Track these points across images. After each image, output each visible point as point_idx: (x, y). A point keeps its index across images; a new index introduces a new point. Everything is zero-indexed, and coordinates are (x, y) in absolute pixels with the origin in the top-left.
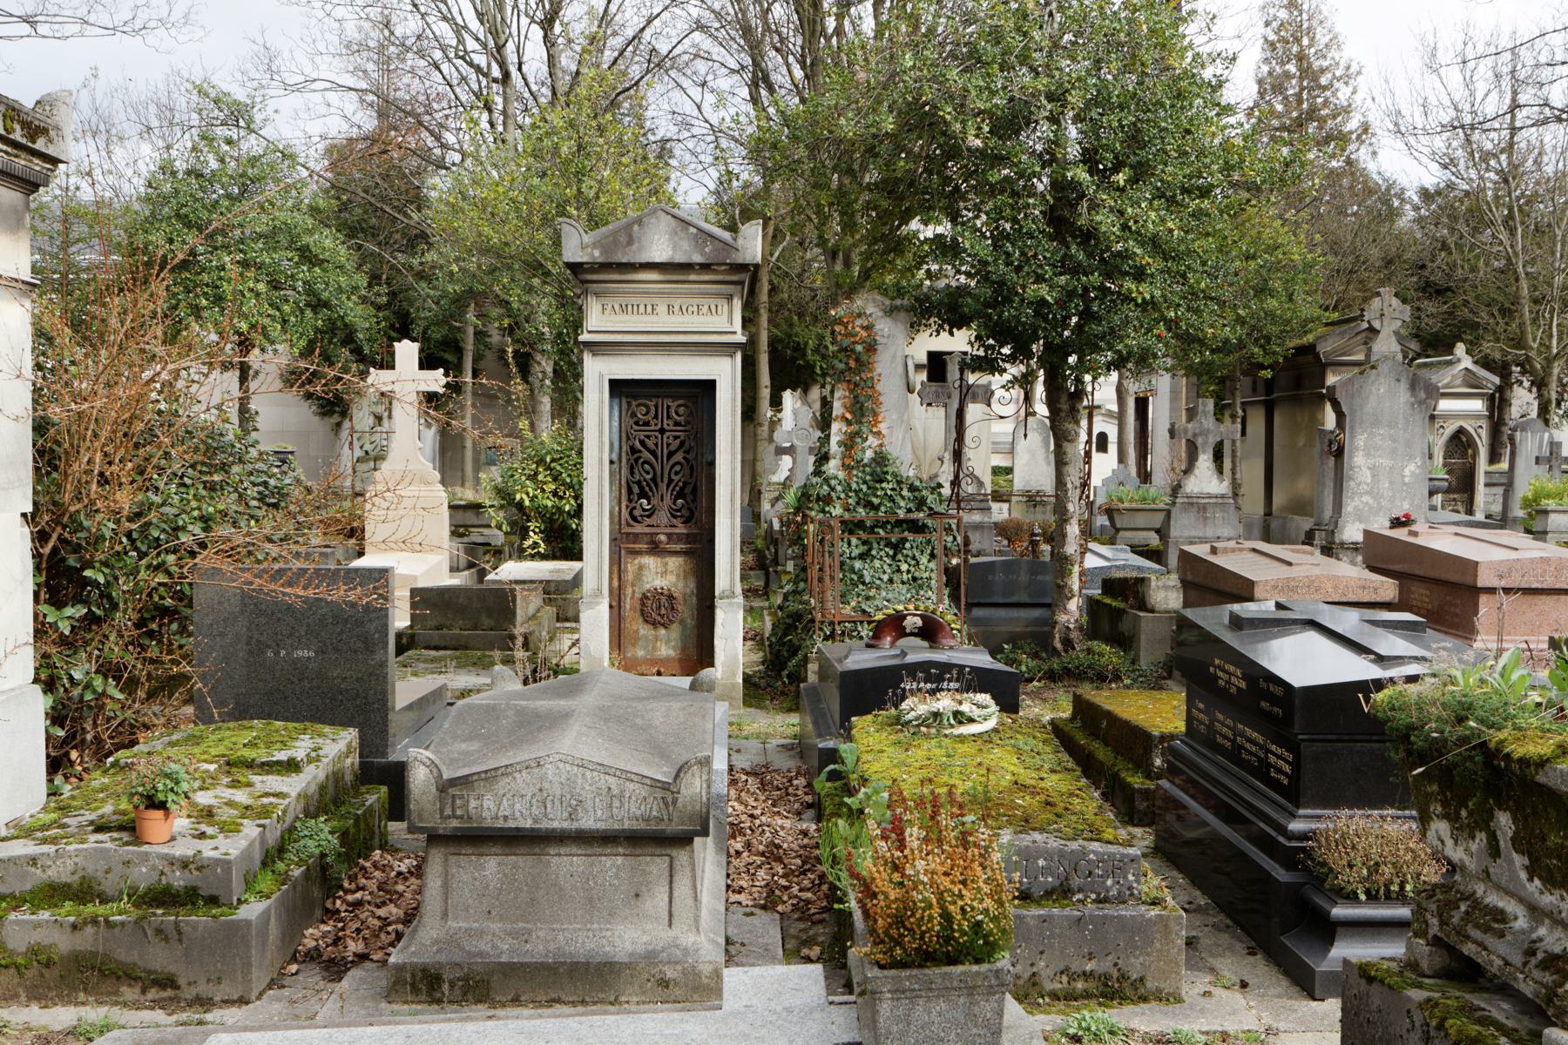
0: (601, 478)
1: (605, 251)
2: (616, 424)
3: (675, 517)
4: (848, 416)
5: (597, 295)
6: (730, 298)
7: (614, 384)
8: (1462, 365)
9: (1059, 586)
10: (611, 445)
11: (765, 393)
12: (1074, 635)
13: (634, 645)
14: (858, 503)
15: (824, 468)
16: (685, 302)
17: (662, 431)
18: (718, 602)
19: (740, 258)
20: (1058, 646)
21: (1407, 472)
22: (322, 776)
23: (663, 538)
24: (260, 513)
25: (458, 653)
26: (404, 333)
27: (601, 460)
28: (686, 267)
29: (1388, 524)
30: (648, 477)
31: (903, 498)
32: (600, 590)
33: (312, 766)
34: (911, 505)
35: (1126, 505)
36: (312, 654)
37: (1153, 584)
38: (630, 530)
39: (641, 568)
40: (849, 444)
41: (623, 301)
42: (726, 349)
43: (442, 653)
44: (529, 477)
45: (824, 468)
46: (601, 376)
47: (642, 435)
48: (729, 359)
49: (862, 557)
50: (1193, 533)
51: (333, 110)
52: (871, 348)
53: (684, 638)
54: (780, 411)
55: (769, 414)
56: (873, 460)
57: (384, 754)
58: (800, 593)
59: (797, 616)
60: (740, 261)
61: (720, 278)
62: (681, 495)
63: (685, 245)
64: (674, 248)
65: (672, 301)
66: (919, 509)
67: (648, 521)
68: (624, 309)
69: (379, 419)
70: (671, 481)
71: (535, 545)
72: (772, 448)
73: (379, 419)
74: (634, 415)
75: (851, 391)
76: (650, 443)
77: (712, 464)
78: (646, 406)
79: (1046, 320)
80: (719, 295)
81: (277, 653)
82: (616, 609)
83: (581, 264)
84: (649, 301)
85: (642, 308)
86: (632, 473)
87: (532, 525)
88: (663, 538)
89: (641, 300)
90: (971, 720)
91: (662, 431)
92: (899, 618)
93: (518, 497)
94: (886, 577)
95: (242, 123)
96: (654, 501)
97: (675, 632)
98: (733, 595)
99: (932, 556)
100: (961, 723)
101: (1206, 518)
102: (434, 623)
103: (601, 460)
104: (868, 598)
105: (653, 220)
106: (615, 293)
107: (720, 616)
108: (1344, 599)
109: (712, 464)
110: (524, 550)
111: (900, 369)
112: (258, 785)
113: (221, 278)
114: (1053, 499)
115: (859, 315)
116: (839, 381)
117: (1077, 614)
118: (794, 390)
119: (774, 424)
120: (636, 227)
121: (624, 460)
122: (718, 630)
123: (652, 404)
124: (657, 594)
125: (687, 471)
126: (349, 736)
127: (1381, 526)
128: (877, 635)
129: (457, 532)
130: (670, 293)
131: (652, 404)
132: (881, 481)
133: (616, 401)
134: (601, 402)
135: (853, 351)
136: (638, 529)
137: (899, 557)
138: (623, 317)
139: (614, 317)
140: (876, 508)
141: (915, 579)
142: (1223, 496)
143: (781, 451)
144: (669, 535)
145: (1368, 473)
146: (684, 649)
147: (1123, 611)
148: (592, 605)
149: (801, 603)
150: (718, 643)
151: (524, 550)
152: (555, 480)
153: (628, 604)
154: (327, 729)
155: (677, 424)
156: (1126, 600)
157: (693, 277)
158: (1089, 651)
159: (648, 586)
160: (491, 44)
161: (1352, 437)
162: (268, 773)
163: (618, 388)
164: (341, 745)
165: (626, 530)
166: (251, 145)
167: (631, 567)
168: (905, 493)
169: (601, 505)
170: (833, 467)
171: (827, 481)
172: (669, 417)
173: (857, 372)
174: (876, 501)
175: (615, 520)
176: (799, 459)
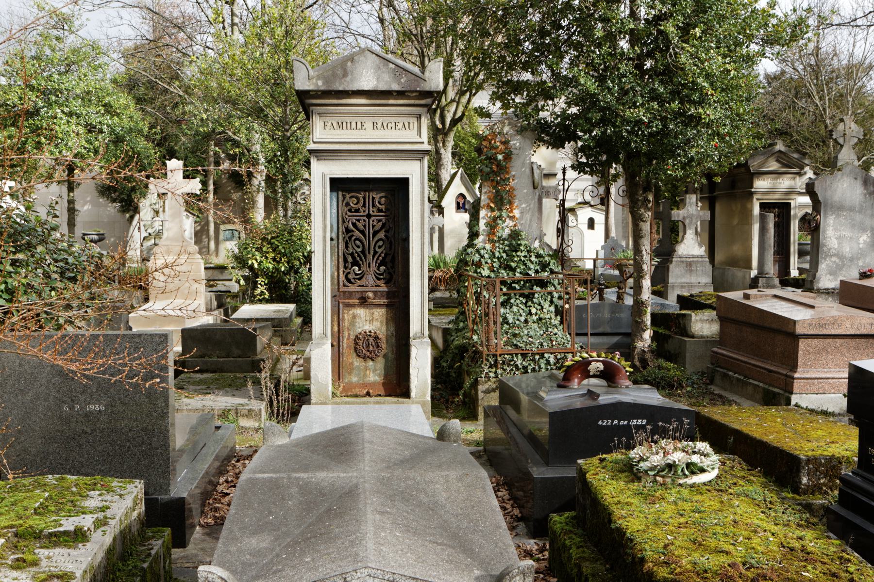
1: (326, 81)
2: (335, 211)
3: (379, 279)
4: (492, 205)
5: (320, 115)
8: (807, 176)
9: (637, 322)
10: (332, 226)
12: (648, 356)
13: (350, 373)
14: (500, 266)
15: (475, 242)
17: (369, 216)
19: (427, 87)
21: (861, 240)
22: (108, 540)
23: (371, 295)
24: (59, 285)
25: (216, 375)
26: (172, 154)
29: (858, 276)
30: (359, 250)
31: (532, 262)
32: (325, 333)
33: (99, 532)
34: (538, 267)
36: (102, 408)
37: (693, 318)
38: (346, 289)
39: (354, 317)
40: (493, 225)
41: (340, 119)
43: (206, 375)
44: (257, 249)
45: (475, 242)
46: (324, 176)
49: (504, 304)
50: (684, 280)
51: (124, 21)
52: (508, 157)
53: (386, 368)
56: (510, 235)
57: (167, 491)
60: (427, 89)
63: (386, 77)
65: (376, 119)
66: (544, 270)
67: (359, 282)
68: (340, 125)
69: (157, 212)
70: (375, 252)
71: (262, 293)
73: (157, 212)
74: (348, 204)
76: (360, 225)
77: (406, 240)
78: (357, 198)
79: (637, 135)
80: (410, 115)
81: (72, 408)
82: (337, 347)
83: (308, 92)
84: (359, 120)
85: (354, 125)
86: (347, 247)
87: (259, 280)
88: (371, 295)
89: (354, 119)
90: (703, 470)
91: (369, 216)
92: (586, 363)
93: (250, 262)
94: (522, 319)
95: (66, 27)
96: (364, 268)
97: (380, 363)
99: (552, 302)
100: (693, 473)
101: (691, 271)
104: (515, 335)
105: (362, 58)
107: (414, 352)
108: (858, 333)
110: (255, 297)
111: (528, 171)
112: (44, 563)
114: (631, 262)
116: (486, 180)
117: (649, 342)
120: (349, 64)
122: (413, 362)
123: (361, 196)
124: (367, 335)
125: (388, 246)
126: (136, 488)
127: (852, 276)
128: (567, 378)
129: (210, 283)
131: (361, 196)
132: (516, 251)
133: (335, 194)
134: (324, 194)
135: (496, 159)
137: (530, 303)
138: (340, 132)
139: (332, 131)
140: (514, 270)
141: (540, 319)
142: (702, 257)
144: (375, 293)
145: (835, 241)
146: (386, 376)
147: (669, 337)
148: (319, 345)
149: (464, 338)
150: (413, 371)
151: (255, 297)
152: (274, 250)
153: (345, 344)
154: (115, 483)
155: (379, 211)
156: (668, 328)
157: (391, 102)
158: (660, 368)
159: (360, 330)
161: (826, 217)
162: (56, 545)
163: (338, 185)
164: (128, 502)
165: (342, 289)
166: (71, 40)
168: (533, 258)
169: (324, 271)
170: (479, 242)
171: (478, 251)
172: (373, 206)
173: (497, 174)
174: (513, 265)
175: (336, 282)
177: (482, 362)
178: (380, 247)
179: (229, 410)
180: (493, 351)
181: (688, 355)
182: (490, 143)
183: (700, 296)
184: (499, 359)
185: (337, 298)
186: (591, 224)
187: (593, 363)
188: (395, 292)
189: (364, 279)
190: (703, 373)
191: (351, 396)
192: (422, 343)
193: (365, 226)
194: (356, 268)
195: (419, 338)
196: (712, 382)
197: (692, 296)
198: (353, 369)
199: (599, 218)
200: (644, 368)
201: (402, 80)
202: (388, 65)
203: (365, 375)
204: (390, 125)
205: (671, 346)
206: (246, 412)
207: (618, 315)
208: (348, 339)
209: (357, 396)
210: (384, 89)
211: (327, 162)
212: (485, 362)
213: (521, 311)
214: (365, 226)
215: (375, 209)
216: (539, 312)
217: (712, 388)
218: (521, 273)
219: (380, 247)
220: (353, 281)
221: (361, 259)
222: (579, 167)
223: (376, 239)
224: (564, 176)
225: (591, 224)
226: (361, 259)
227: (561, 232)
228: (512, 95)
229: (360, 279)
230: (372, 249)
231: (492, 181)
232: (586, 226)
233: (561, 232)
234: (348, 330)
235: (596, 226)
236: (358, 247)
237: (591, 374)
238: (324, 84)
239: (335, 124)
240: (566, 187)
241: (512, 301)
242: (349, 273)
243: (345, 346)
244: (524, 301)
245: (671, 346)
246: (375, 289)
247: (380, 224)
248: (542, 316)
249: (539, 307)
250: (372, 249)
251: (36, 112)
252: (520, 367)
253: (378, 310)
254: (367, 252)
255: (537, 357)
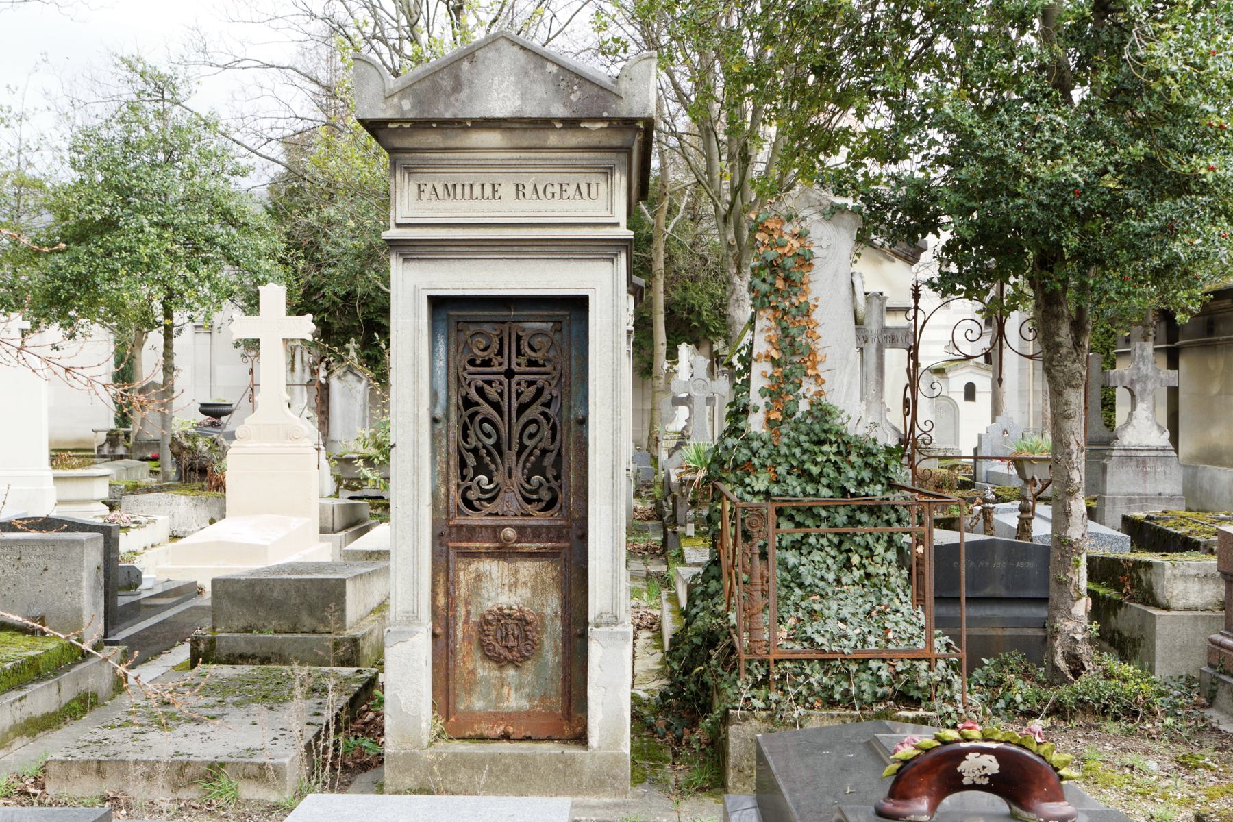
0: (416, 444)
1: (419, 103)
3: (529, 501)
6: (608, 172)
7: (437, 303)
11: (661, 349)
13: (469, 692)
16: (542, 180)
17: (510, 374)
18: (593, 632)
20: (1062, 664)
23: (510, 533)
27: (416, 416)
28: (544, 123)
30: (490, 442)
35: (1036, 456)
37: (1168, 572)
38: (462, 521)
41: (450, 179)
42: (602, 249)
46: (416, 291)
47: (479, 380)
48: (608, 264)
49: (797, 545)
52: (805, 260)
54: (676, 363)
55: (666, 366)
58: (712, 596)
59: (711, 639)
60: (624, 114)
61: (593, 140)
62: (538, 468)
63: (541, 91)
64: (523, 96)
65: (521, 179)
67: (489, 507)
68: (450, 190)
70: (522, 448)
72: (669, 398)
75: (779, 321)
76: (492, 393)
80: (592, 168)
83: (383, 123)
84: (488, 180)
85: (477, 190)
86: (465, 436)
89: (477, 179)
94: (831, 577)
95: (167, 96)
98: (615, 621)
101: (1146, 473)
102: (241, 623)
103: (416, 416)
105: (492, 54)
106: (436, 166)
107: (595, 651)
109: (583, 422)
111: (845, 290)
113: (139, 240)
115: (789, 219)
116: (763, 307)
118: (689, 343)
119: (669, 375)
120: (466, 65)
121: (453, 417)
124: (501, 616)
130: (518, 167)
132: (820, 443)
136: (475, 519)
137: (846, 546)
138: (449, 203)
139: (435, 204)
142: (1164, 449)
143: (677, 402)
144: (520, 530)
147: (1120, 604)
148: (403, 636)
149: (714, 614)
156: (1118, 587)
158: (1108, 675)
159: (490, 604)
160: (404, 22)
167: (464, 575)
169: (416, 484)
170: (755, 424)
171: (748, 440)
172: (519, 353)
174: (815, 470)
176: (696, 409)
177: (738, 674)
178: (531, 436)
179: (222, 765)
180: (761, 653)
181: (1158, 643)
182: (771, 235)
183: (1166, 520)
184: (773, 669)
185: (445, 539)
186: (970, 392)
187: (970, 756)
188: (562, 527)
189: (498, 500)
190: (1190, 680)
191: (471, 739)
192: (612, 635)
193: (501, 394)
194: (484, 478)
195: (607, 624)
196: (1211, 701)
197: (1148, 518)
198: (476, 683)
199: (984, 384)
200: (1076, 674)
201: (572, 97)
202: (543, 67)
203: (499, 697)
204: (549, 189)
205: (1124, 621)
206: (255, 770)
207: (1020, 565)
208: (466, 622)
209: (482, 739)
210: (534, 115)
211: (423, 264)
212: (744, 675)
213: (830, 561)
214: (501, 394)
215: (522, 360)
216: (865, 562)
217: (1213, 715)
218: (829, 486)
219: (531, 436)
220: (476, 504)
221: (494, 461)
222: (945, 286)
223: (523, 420)
224: (916, 301)
225: (970, 392)
226: (494, 461)
227: (910, 406)
228: (822, 157)
229: (490, 500)
230: (515, 441)
231: (775, 308)
232: (963, 395)
233: (910, 406)
234: (467, 603)
235: (977, 395)
236: (489, 436)
237: (966, 781)
238: (414, 106)
239: (440, 189)
240: (920, 323)
241: (812, 540)
242: (469, 488)
243: (460, 635)
244: (836, 540)
245: (1124, 621)
246: (519, 521)
247: (533, 389)
248: (871, 569)
249: (866, 553)
250: (515, 441)
251: (109, 225)
252: (817, 688)
253: (527, 564)
254: (505, 447)
255: (853, 668)
